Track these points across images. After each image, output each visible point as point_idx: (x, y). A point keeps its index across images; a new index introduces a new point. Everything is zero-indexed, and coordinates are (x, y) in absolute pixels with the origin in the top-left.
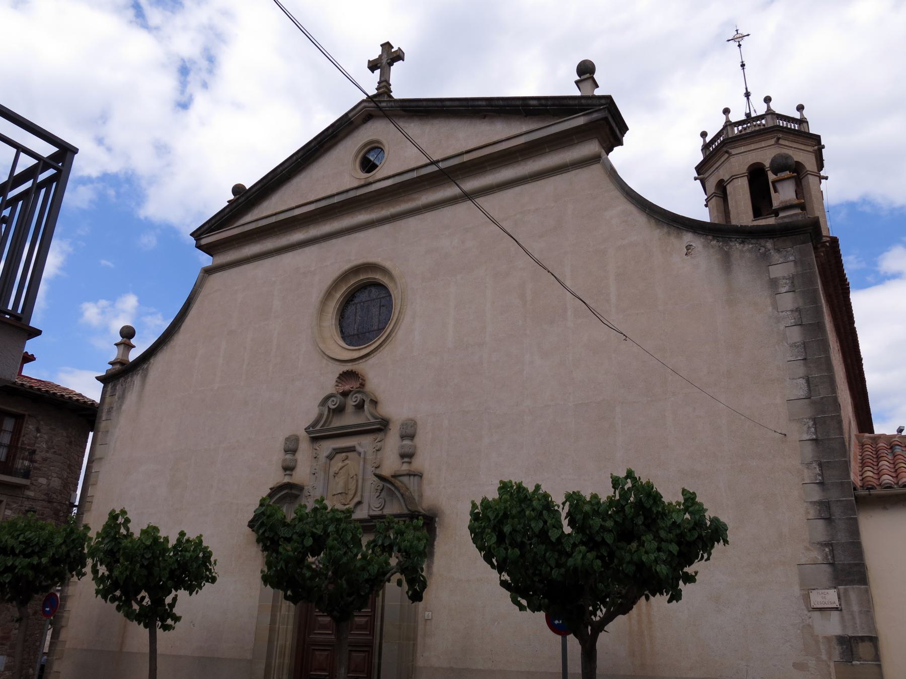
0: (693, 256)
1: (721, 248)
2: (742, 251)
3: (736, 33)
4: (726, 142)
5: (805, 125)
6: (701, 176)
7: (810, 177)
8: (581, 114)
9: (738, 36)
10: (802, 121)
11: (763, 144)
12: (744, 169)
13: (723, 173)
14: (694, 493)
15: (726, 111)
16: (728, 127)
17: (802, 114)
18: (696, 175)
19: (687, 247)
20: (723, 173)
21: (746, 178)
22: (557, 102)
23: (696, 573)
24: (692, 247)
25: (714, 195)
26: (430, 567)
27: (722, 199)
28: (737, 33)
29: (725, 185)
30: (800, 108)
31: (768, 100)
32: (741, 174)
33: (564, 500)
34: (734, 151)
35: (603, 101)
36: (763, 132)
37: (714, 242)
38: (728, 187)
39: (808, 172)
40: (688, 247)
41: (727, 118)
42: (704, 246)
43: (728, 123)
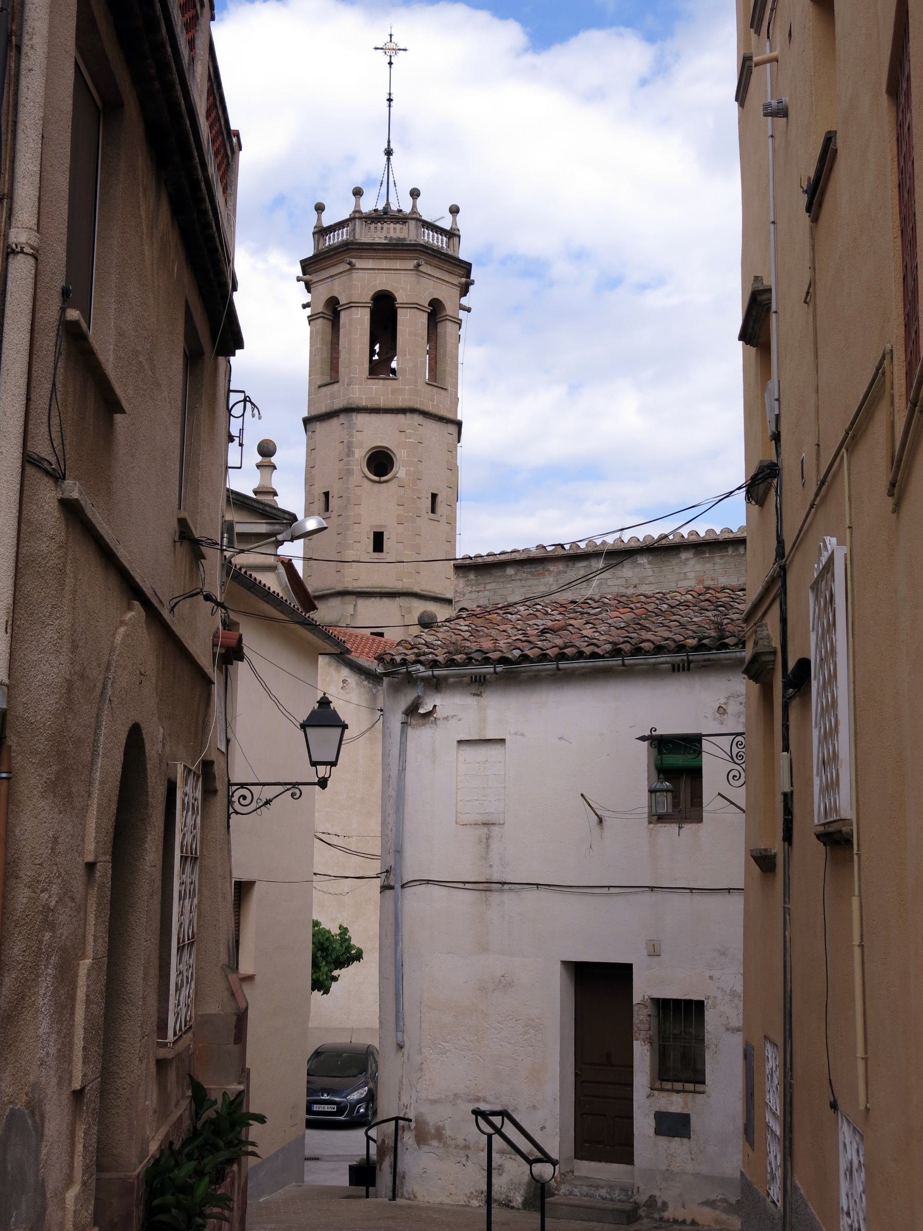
0: (347, 691)
3: (389, 41)
4: (350, 247)
5: (456, 239)
6: (307, 277)
7: (448, 323)
8: (264, 521)
9: (392, 45)
10: (452, 235)
11: (398, 264)
12: (367, 298)
13: (338, 288)
14: (347, 928)
15: (320, 208)
16: (357, 220)
17: (454, 222)
18: (301, 274)
19: (343, 681)
20: (338, 288)
21: (368, 310)
22: (241, 499)
23: (339, 976)
24: (347, 682)
25: (321, 315)
26: (488, 1111)
27: (330, 324)
28: (391, 41)
29: (339, 309)
30: (454, 210)
31: (415, 194)
32: (363, 303)
33: (529, 1167)
34: (358, 263)
35: (287, 516)
36: (400, 248)
37: (366, 683)
38: (343, 315)
39: (448, 318)
40: (344, 681)
41: (357, 204)
42: (357, 684)
43: (357, 215)
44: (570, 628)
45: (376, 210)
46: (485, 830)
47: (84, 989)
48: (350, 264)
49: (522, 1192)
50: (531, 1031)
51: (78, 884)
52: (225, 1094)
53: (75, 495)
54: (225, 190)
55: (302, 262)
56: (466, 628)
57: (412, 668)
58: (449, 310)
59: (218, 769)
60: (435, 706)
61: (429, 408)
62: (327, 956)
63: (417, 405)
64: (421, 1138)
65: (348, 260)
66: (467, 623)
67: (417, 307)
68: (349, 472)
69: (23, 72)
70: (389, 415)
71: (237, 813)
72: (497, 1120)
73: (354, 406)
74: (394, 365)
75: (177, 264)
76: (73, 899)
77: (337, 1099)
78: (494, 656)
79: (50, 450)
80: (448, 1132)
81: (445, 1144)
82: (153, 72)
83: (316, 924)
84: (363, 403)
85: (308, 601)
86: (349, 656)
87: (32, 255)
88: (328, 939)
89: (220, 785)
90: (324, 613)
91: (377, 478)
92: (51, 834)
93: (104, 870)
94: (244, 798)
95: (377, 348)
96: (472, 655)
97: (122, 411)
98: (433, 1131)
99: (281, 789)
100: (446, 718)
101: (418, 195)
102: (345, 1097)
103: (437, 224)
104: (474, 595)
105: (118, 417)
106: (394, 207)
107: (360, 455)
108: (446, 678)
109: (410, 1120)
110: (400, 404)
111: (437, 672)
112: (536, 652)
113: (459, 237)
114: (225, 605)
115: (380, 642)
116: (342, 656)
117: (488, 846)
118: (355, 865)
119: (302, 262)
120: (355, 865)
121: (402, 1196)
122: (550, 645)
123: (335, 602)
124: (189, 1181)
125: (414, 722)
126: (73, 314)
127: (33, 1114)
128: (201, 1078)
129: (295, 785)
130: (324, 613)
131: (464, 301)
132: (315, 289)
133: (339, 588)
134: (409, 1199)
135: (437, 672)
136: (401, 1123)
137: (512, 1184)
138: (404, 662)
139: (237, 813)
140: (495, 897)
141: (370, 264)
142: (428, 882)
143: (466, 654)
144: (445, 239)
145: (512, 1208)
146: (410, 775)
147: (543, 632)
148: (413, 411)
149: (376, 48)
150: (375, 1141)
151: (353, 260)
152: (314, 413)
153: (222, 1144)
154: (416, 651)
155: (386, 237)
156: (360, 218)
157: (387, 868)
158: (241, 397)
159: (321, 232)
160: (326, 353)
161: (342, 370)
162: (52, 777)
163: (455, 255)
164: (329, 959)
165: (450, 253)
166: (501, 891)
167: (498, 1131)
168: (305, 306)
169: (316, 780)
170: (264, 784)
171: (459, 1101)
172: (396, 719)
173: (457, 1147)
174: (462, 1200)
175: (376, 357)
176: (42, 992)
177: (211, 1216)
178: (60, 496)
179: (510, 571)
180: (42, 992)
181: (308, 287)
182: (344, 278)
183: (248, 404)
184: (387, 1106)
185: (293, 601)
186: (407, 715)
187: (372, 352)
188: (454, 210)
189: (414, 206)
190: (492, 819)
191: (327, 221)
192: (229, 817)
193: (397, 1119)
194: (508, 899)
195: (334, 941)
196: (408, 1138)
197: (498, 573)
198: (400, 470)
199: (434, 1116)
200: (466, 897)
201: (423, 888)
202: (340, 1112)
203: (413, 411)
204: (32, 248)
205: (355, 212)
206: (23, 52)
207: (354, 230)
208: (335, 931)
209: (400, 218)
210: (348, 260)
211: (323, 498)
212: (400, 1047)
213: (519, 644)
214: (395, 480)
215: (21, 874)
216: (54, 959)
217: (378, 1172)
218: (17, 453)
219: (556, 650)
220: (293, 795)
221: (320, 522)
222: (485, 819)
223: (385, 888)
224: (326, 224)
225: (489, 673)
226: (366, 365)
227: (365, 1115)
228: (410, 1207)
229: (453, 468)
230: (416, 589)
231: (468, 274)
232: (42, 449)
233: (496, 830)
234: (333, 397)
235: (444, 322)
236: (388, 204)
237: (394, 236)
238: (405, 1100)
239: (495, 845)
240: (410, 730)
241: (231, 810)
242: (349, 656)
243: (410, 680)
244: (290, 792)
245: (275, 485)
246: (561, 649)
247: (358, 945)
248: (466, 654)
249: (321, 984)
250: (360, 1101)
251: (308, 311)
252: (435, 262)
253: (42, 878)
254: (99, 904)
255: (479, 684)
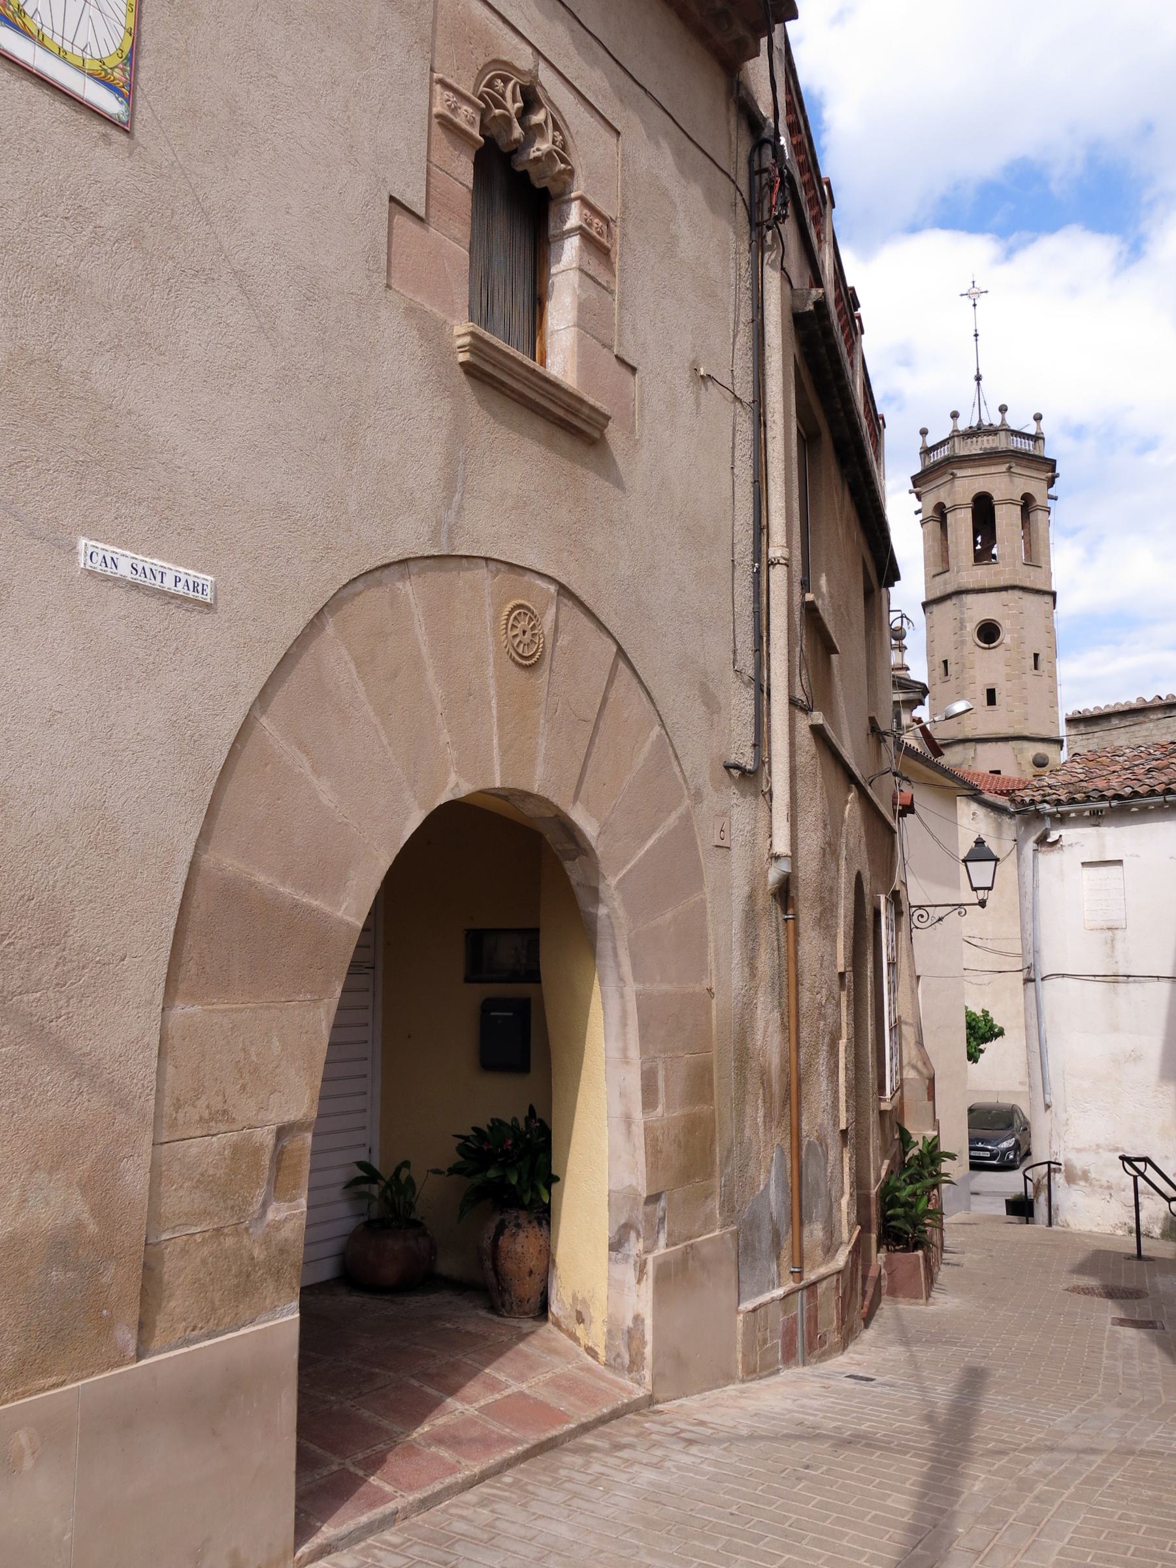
1: (996, 820)
2: (1010, 824)
5: (1041, 442)
9: (974, 290)
11: (993, 469)
12: (968, 500)
13: (942, 495)
15: (924, 432)
17: (1039, 427)
18: (912, 488)
20: (942, 495)
30: (1038, 418)
31: (1003, 409)
34: (959, 473)
35: (918, 686)
37: (992, 814)
38: (949, 516)
40: (974, 814)
41: (955, 425)
43: (956, 434)
44: (1172, 766)
45: (971, 427)
46: (1110, 933)
47: (844, 1060)
48: (952, 474)
49: (1160, 1225)
50: (1160, 1096)
51: (836, 988)
52: (924, 1137)
53: (821, 722)
54: (877, 460)
55: (912, 478)
56: (1081, 771)
57: (1040, 807)
58: (1040, 500)
59: (902, 895)
60: (1061, 836)
61: (1027, 584)
62: (974, 1033)
63: (1017, 583)
64: (1071, 1179)
65: (950, 471)
66: (1081, 766)
67: (1011, 502)
68: (963, 643)
69: (769, 439)
70: (993, 594)
71: (917, 928)
72: (1140, 1165)
73: (963, 589)
74: (994, 551)
75: (857, 533)
76: (834, 998)
77: (989, 1147)
78: (1109, 793)
79: (802, 692)
80: (1093, 1175)
81: (1091, 1184)
82: (839, 406)
83: (966, 1008)
84: (971, 586)
85: (936, 748)
86: (982, 796)
87: (785, 564)
88: (974, 1020)
89: (905, 908)
90: (950, 758)
91: (986, 646)
92: (820, 954)
93: (849, 977)
94: (922, 916)
95: (979, 539)
96: (1090, 794)
97: (837, 652)
98: (1080, 1173)
99: (950, 909)
100: (1071, 845)
101: (1006, 410)
102: (996, 1146)
103: (1023, 431)
104: (1084, 742)
105: (834, 657)
106: (986, 422)
107: (971, 628)
108: (1068, 813)
109: (1060, 1164)
110: (1002, 583)
111: (1060, 809)
112: (1147, 788)
113: (1043, 439)
114: (910, 778)
115: (999, 779)
116: (975, 795)
117: (1113, 947)
118: (993, 961)
119: (912, 478)
120: (993, 961)
121: (1057, 1224)
122: (1156, 782)
123: (958, 749)
124: (910, 1199)
125: (1043, 849)
126: (809, 597)
127: (822, 1145)
128: (907, 1126)
129: (960, 905)
130: (950, 758)
131: (1051, 491)
132: (925, 498)
133: (960, 737)
134: (1063, 1226)
135: (1060, 809)
136: (1053, 1166)
137: (1151, 1218)
138: (1033, 802)
139: (917, 928)
140: (1121, 987)
141: (969, 472)
142: (1063, 975)
143: (1085, 793)
144: (1031, 443)
145: (1152, 1237)
146: (1042, 892)
147: (1149, 771)
148: (1014, 588)
149: (962, 295)
150: (1031, 1180)
151: (955, 471)
152: (931, 597)
153: (927, 1174)
154: (1042, 792)
155: (981, 449)
156: (958, 436)
157: (1029, 964)
158: (899, 614)
159: (927, 451)
160: (937, 547)
161: (951, 561)
162: (818, 916)
163: (1041, 454)
164: (977, 1035)
165: (1037, 453)
166: (1127, 982)
167: (1142, 1175)
168: (917, 513)
169: (977, 901)
170: (936, 906)
171: (1101, 1151)
172: (1030, 845)
173: (1101, 1187)
174: (1108, 1230)
175: (979, 547)
176: (821, 1062)
177: (928, 1225)
178: (810, 723)
179: (1115, 722)
180: (821, 1062)
181: (919, 497)
182: (948, 486)
183: (904, 619)
184: (1040, 1152)
185: (929, 754)
186: (1038, 844)
187: (975, 543)
188: (1038, 418)
189: (1003, 419)
190: (1115, 925)
191: (931, 441)
192: (911, 931)
193: (1049, 1163)
194: (1133, 988)
195: (980, 1021)
196: (1059, 1179)
197: (1105, 726)
198: (1006, 637)
199: (1080, 1162)
200: (1100, 987)
201: (1059, 980)
202: (993, 1157)
203: (1014, 588)
204: (784, 559)
205: (953, 431)
206: (768, 426)
207: (954, 446)
208: (979, 1013)
209: (992, 431)
210: (950, 471)
211: (942, 665)
212: (1048, 1107)
213: (1129, 783)
214: (1002, 645)
215: (804, 982)
216: (827, 1040)
217: (1035, 1204)
218: (786, 701)
219: (1163, 786)
220: (959, 913)
221: (967, 705)
222: (1110, 924)
223: (1027, 981)
224: (929, 445)
225: (1106, 808)
226: (972, 555)
227: (1014, 1161)
228: (1064, 1233)
229: (1051, 631)
230: (1026, 733)
231: (1053, 470)
232: (799, 694)
233: (1119, 933)
234: (945, 583)
235: (1035, 512)
236: (980, 420)
237: (988, 446)
238: (1055, 1148)
239: (1119, 945)
240: (1040, 856)
241: (913, 926)
242: (982, 796)
243: (1039, 816)
244: (957, 911)
245: (907, 662)
246: (1167, 785)
247: (999, 1025)
248: (1085, 793)
249: (973, 1057)
250: (1009, 1149)
251: (920, 516)
252: (1024, 463)
253: (817, 984)
254: (848, 1001)
255: (1097, 818)
